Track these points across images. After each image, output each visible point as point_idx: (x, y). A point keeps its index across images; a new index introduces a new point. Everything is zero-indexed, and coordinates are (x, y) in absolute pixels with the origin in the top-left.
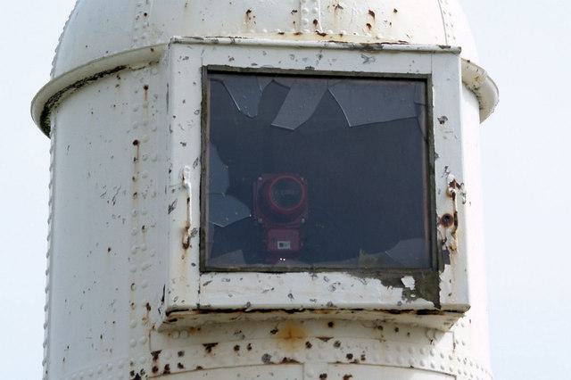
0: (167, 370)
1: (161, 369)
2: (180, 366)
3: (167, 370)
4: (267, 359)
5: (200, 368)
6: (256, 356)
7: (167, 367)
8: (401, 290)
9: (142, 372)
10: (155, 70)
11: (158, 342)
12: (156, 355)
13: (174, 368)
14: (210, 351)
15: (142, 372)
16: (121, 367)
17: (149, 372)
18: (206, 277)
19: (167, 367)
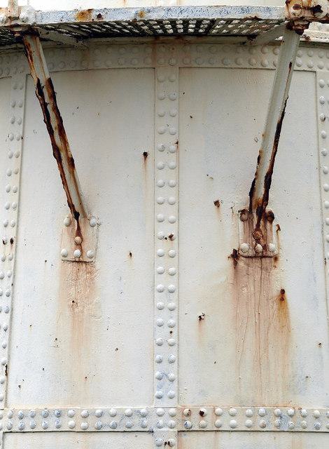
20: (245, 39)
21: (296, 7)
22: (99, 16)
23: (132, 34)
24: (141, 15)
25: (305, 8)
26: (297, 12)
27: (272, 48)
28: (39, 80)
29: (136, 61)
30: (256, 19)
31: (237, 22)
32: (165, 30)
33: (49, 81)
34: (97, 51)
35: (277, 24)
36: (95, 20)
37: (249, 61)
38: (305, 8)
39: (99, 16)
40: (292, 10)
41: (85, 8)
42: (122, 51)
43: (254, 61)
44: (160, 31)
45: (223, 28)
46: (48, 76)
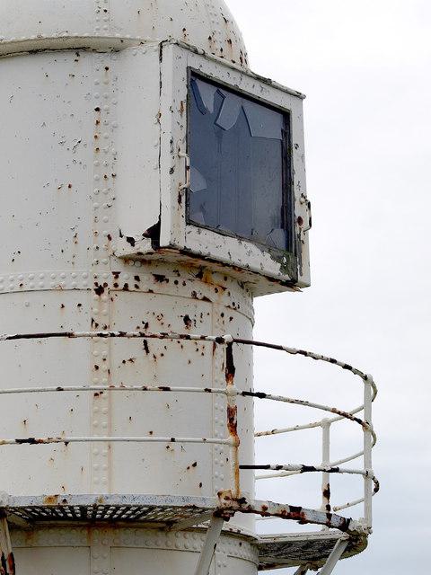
0: (126, 288)
1: (121, 286)
2: (137, 286)
3: (126, 288)
4: (194, 294)
5: (151, 291)
6: (187, 291)
7: (126, 285)
8: (279, 265)
9: (106, 285)
10: (115, 57)
11: (118, 266)
12: (116, 275)
13: (131, 287)
14: (114, 273)
15: (106, 285)
16: (86, 277)
17: (111, 286)
18: (189, 228)
19: (126, 285)
20: (164, 525)
21: (227, 498)
22: (65, 501)
23: (49, 518)
24: (100, 501)
25: (233, 499)
26: (228, 502)
27: (191, 534)
28: (3, 554)
29: (51, 541)
30: (194, 507)
31: (124, 508)
32: (65, 514)
33: (11, 555)
34: (40, 532)
35: (161, 511)
36: (61, 504)
37: (166, 543)
38: (233, 499)
39: (65, 501)
40: (223, 501)
41: (52, 494)
42: (62, 532)
43: (169, 543)
44: (70, 515)
45: (123, 513)
46: (11, 551)
